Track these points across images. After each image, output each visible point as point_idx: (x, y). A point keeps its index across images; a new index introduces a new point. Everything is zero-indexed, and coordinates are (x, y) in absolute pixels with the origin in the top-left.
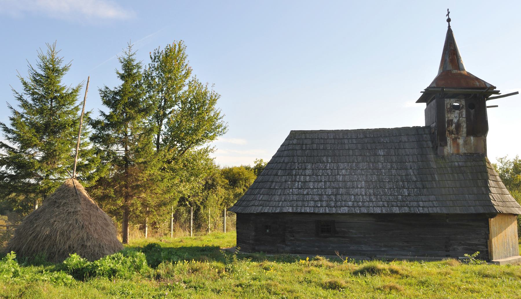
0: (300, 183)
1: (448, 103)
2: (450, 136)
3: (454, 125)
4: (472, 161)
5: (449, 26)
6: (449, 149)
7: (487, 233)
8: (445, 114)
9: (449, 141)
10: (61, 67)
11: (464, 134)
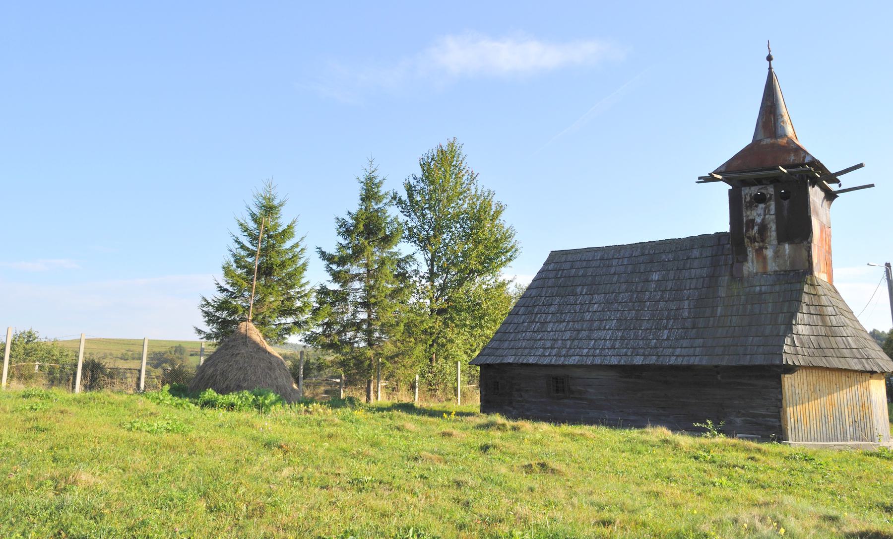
0: (538, 324)
1: (747, 194)
2: (753, 246)
3: (756, 228)
4: (783, 283)
5: (770, 68)
6: (751, 266)
7: (780, 397)
8: (742, 212)
9: (751, 253)
10: (276, 203)
11: (774, 240)
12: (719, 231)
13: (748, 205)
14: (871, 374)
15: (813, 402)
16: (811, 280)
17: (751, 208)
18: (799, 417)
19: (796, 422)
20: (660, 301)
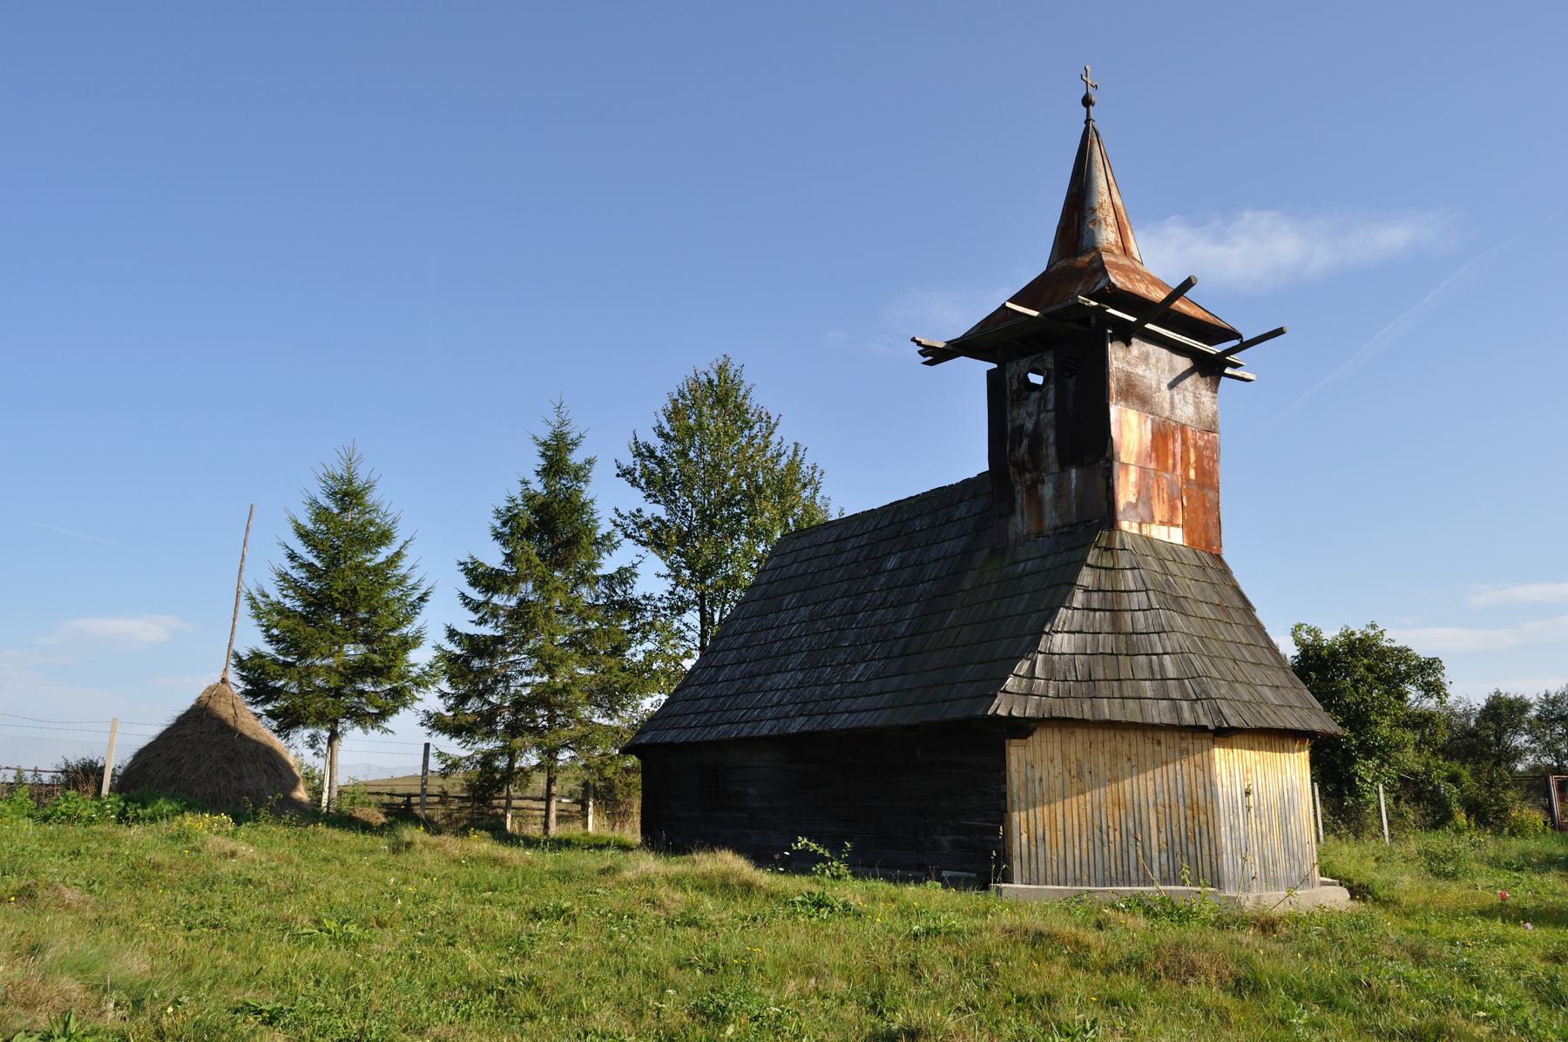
3: (1025, 442)
5: (1087, 121)
13: (1015, 397)
14: (1214, 736)
15: (1074, 799)
16: (1110, 539)
18: (1040, 831)
19: (1033, 843)
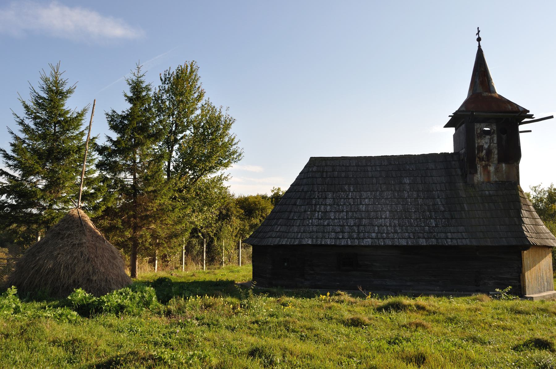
1: (478, 128)
2: (481, 163)
3: (484, 151)
4: (503, 189)
5: (479, 46)
6: (479, 177)
10: (65, 89)
12: (444, 152)
17: (481, 137)
20: (418, 199)
